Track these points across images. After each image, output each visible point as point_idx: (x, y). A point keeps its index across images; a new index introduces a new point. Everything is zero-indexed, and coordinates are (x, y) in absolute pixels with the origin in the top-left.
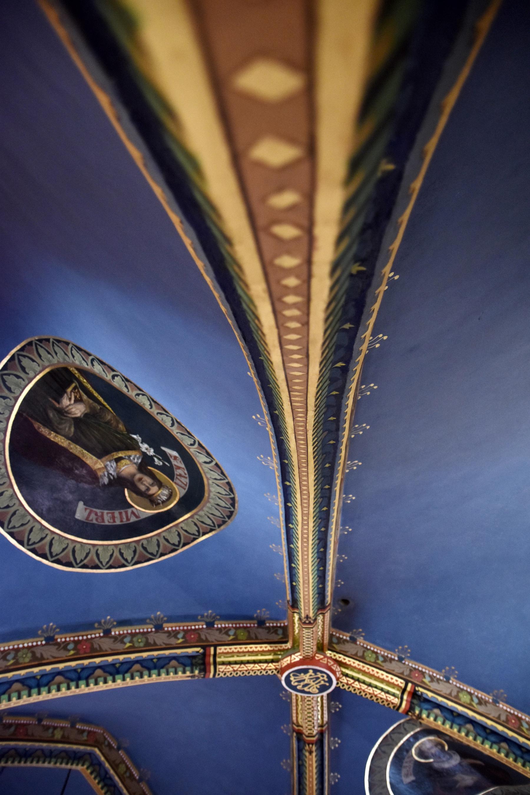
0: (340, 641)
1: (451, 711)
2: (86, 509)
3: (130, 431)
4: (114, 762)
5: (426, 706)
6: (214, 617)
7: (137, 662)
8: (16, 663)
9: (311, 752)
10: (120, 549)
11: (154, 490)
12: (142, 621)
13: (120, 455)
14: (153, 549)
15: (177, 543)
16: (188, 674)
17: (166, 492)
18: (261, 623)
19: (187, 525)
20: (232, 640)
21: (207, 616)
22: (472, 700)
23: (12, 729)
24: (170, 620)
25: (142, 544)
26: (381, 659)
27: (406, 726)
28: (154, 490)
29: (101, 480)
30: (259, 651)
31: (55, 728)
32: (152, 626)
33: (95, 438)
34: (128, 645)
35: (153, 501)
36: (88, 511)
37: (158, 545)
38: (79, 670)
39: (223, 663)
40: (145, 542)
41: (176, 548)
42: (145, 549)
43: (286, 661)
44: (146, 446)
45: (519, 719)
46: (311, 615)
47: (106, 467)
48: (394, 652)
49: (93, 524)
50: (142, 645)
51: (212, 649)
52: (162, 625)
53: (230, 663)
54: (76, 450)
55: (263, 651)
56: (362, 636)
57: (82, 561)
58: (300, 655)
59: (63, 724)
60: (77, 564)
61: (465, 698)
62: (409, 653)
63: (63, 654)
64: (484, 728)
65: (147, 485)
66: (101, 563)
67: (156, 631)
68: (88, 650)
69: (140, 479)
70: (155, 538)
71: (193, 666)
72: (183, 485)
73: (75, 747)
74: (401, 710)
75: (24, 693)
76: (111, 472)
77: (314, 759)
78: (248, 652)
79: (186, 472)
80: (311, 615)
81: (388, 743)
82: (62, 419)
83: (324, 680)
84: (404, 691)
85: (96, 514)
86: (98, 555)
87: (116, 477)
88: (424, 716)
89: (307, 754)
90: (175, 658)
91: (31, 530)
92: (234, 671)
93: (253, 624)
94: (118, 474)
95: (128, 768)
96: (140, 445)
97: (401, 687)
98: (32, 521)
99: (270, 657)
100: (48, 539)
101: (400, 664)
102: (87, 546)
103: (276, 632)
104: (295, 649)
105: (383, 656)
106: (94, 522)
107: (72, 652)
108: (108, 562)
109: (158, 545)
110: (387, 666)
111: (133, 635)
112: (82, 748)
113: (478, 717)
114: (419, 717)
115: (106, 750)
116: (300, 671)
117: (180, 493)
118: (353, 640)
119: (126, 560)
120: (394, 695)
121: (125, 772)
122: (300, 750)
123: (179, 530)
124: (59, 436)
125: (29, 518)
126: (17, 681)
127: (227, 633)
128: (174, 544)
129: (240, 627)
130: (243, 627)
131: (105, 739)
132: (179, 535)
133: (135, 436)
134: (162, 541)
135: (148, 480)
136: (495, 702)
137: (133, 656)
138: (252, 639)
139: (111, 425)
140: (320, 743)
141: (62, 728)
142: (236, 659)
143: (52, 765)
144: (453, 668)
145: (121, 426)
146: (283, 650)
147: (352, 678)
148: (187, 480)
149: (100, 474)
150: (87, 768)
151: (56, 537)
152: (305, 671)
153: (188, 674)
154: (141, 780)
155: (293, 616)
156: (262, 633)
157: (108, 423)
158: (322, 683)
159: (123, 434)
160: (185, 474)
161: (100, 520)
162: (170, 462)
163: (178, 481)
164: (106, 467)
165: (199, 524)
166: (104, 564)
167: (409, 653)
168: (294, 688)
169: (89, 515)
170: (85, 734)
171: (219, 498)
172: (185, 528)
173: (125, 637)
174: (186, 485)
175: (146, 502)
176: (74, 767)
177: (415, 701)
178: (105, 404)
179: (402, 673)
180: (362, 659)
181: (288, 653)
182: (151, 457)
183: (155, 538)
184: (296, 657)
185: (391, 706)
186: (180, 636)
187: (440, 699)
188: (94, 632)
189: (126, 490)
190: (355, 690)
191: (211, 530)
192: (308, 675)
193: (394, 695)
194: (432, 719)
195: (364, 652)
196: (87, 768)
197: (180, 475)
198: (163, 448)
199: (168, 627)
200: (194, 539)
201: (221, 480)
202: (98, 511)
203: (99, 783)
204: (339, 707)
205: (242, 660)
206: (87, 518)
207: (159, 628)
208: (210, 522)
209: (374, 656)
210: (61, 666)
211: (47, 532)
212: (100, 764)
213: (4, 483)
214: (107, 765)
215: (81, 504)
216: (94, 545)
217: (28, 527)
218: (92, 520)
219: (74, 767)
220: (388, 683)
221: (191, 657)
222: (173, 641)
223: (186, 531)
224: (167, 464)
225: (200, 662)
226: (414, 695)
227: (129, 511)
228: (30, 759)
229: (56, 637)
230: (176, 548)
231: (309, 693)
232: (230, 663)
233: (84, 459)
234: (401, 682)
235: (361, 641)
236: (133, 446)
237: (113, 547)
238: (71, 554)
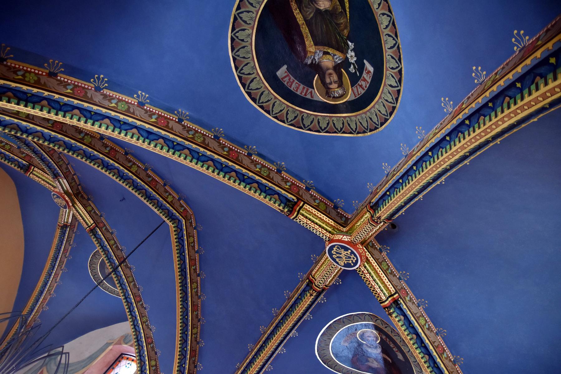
0: (373, 246)
1: (410, 322)
2: (286, 72)
3: (349, 38)
4: (189, 233)
5: (398, 311)
6: (312, 186)
7: (257, 182)
8: (193, 138)
9: (311, 295)
11: (334, 86)
12: (272, 162)
13: (329, 51)
14: (307, 122)
15: (323, 128)
16: (281, 208)
17: (340, 92)
18: (336, 207)
19: (337, 120)
20: (315, 205)
21: (308, 183)
22: (425, 324)
23: (150, 179)
24: (287, 171)
26: (389, 271)
27: (367, 317)
28: (334, 86)
29: (306, 59)
30: (326, 221)
31: (170, 194)
32: (276, 168)
33: (322, 30)
34: (258, 169)
35: (328, 93)
36: (286, 74)
38: (224, 166)
39: (303, 215)
40: (305, 115)
42: (302, 119)
43: (340, 237)
44: (353, 54)
45: (444, 351)
46: (383, 218)
47: (315, 53)
48: (399, 273)
49: (284, 85)
50: (265, 174)
51: (302, 203)
52: (281, 171)
53: (306, 217)
54: (305, 30)
55: (328, 223)
56: (387, 252)
57: (263, 103)
59: (175, 195)
61: (422, 322)
62: (407, 278)
63: (220, 151)
64: (422, 342)
66: (273, 111)
67: (276, 173)
68: (235, 158)
69: (330, 74)
70: (313, 117)
71: (286, 205)
72: (357, 94)
73: (174, 211)
74: (382, 305)
75: (189, 158)
76: (316, 58)
77: (310, 300)
78: (320, 218)
79: (368, 86)
80: (383, 218)
81: (350, 319)
82: (310, 5)
83: (352, 261)
84: (392, 295)
86: (274, 105)
88: (394, 315)
89: (309, 295)
90: (279, 194)
91: (247, 64)
92: (306, 223)
93: (332, 205)
94: (320, 62)
95: (194, 241)
96: (349, 51)
97: (391, 293)
98: (251, 58)
99: (330, 229)
100: (253, 76)
101: (398, 280)
103: (341, 218)
104: (347, 233)
105: (391, 270)
106: (285, 83)
107: (225, 153)
108: (276, 113)
110: (391, 277)
111: (263, 166)
112: (178, 214)
113: (423, 335)
114: (390, 314)
115: (188, 224)
116: (343, 247)
117: (349, 97)
118: (380, 251)
119: (287, 119)
120: (384, 294)
121: (192, 243)
122: (304, 291)
124: (300, 15)
125: (250, 55)
126: (188, 149)
127: (314, 200)
128: (321, 128)
129: (323, 202)
130: (325, 203)
131: (191, 219)
132: (328, 124)
133: (350, 43)
134: (316, 121)
135: (335, 77)
136: (437, 334)
137: (257, 178)
138: (326, 212)
139: (339, 27)
140: (319, 294)
141: (173, 197)
142: (311, 217)
143: (158, 213)
145: (346, 32)
146: (340, 230)
147: (368, 270)
148: (363, 92)
149: (309, 55)
150: (174, 227)
151: (258, 79)
152: (346, 249)
153: (281, 208)
154: (197, 252)
155: (365, 213)
156: (333, 213)
157: (338, 25)
158: (350, 262)
159: (342, 38)
160: (366, 87)
162: (361, 73)
163: (355, 89)
164: (315, 53)
165: (346, 124)
167: (407, 278)
168: (331, 255)
169: (285, 77)
170: (183, 209)
171: (376, 115)
172: (335, 122)
173: (258, 164)
174: (359, 94)
175: (324, 91)
176: (168, 222)
177: (394, 305)
178: (348, 10)
179: (397, 286)
180: (380, 264)
181: (341, 232)
182: (350, 64)
183: (313, 117)
184: (346, 238)
185: (379, 299)
186: (289, 184)
187: (409, 312)
188: (242, 150)
190: (364, 278)
191: (351, 133)
192: (346, 252)
193: (384, 294)
194: (397, 319)
195: (383, 261)
196: (174, 227)
197: (361, 86)
198: (365, 61)
199: (284, 174)
200: (335, 132)
201: (391, 103)
202: (292, 78)
203: (176, 238)
204: (339, 283)
205: (313, 220)
206: (282, 79)
207: (279, 172)
208: (354, 127)
209: (387, 267)
210: (216, 157)
211: (255, 71)
212: (181, 230)
213: (250, 24)
214: (185, 232)
215: (285, 67)
216: (276, 98)
217: (246, 61)
219: (168, 222)
220: (385, 286)
221: (288, 200)
222: (283, 184)
223: (334, 124)
224: (358, 73)
225: (291, 206)
226: (396, 302)
227: (310, 90)
228: (150, 201)
229: (221, 138)
231: (337, 263)
232: (306, 217)
233: (305, 40)
234: (393, 290)
235: (384, 254)
236: (343, 50)
238: (259, 94)
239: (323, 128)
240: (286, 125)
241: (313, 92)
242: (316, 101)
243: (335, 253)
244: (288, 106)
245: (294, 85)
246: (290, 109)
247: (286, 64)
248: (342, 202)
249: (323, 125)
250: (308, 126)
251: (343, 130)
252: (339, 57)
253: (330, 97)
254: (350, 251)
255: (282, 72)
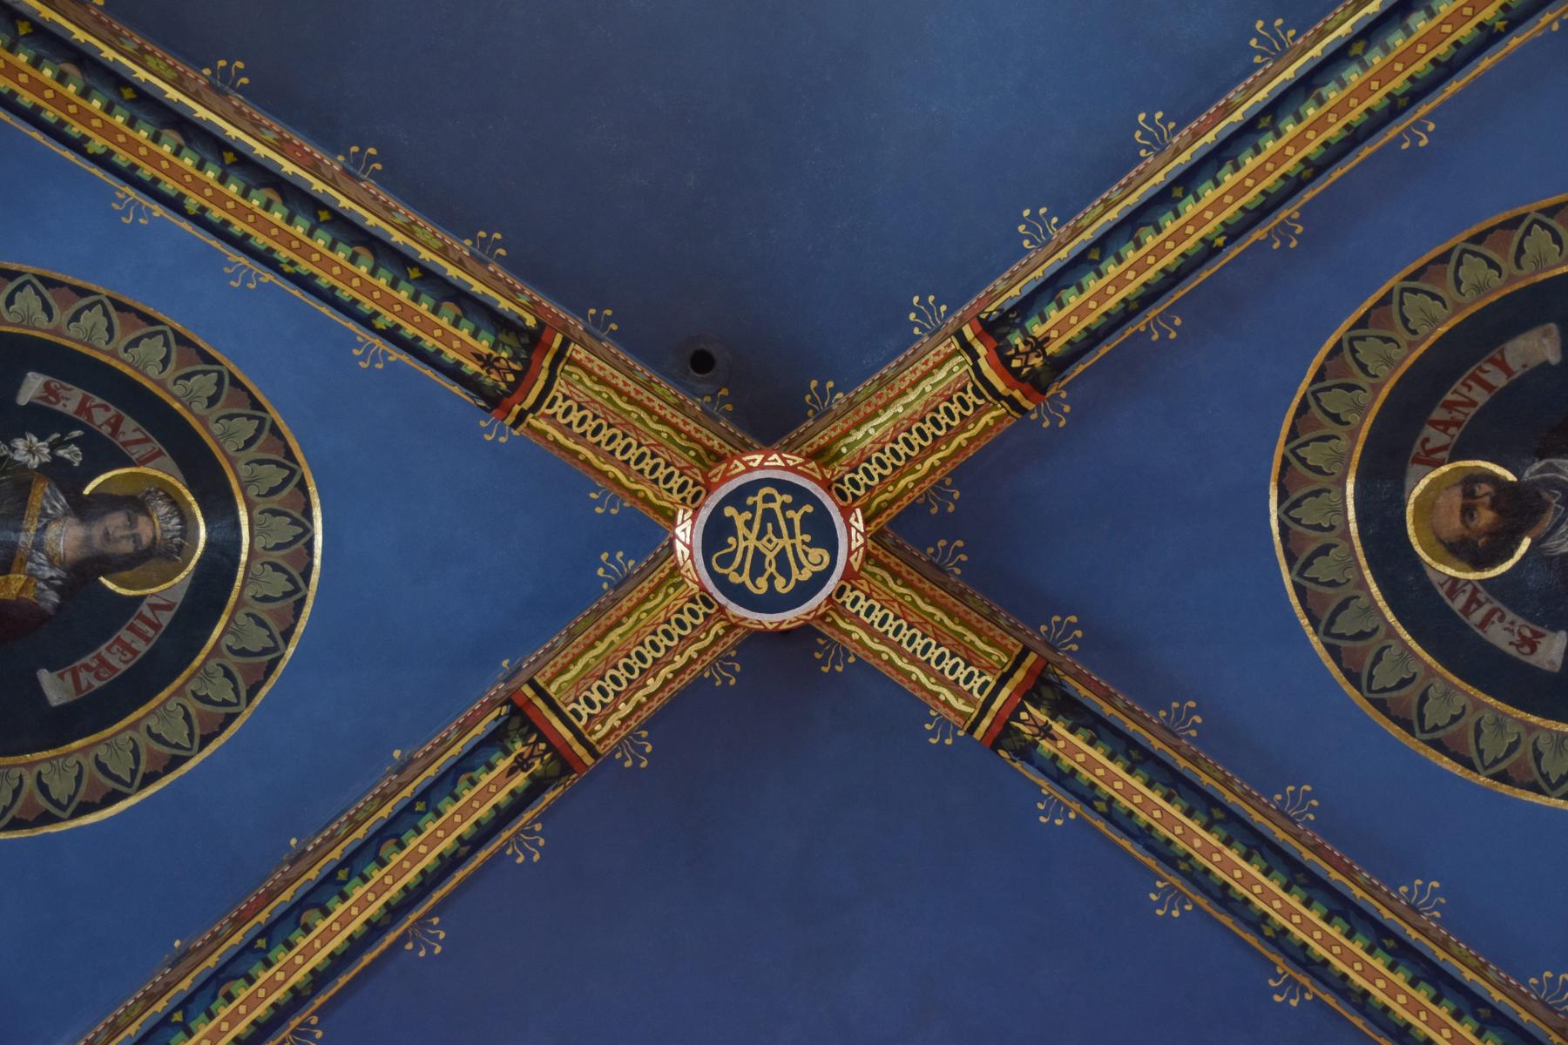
2: (61, 676)
10: (194, 693)
15: (290, 587)
17: (163, 509)
25: (229, 648)
29: (42, 604)
36: (68, 677)
37: (261, 623)
40: (230, 640)
41: (298, 596)
42: (243, 652)
56: (834, 391)
57: (134, 773)
58: (685, 511)
60: (129, 785)
65: (127, 533)
66: (178, 746)
83: (785, 507)
85: (87, 668)
86: (158, 738)
87: (64, 575)
102: (122, 736)
106: (97, 684)
108: (191, 735)
109: (261, 623)
119: (225, 703)
123: (266, 559)
128: (286, 595)
132: (276, 567)
134: (261, 609)
144: (1026, 213)
158: (796, 517)
161: (104, 673)
166: (187, 745)
167: (938, 303)
174: (147, 440)
189: (102, 579)
202: (87, 659)
215: (45, 676)
218: (90, 685)
223: (278, 547)
227: (144, 609)
230: (298, 596)
237: (175, 700)
239: (290, 587)
240: (247, 713)
241: (154, 600)
242: (187, 595)
243: (762, 583)
244: (179, 692)
245: (114, 661)
246: (191, 686)
247: (34, 670)
248: (611, 559)
249: (280, 584)
250: (271, 636)
251: (297, 515)
252: (44, 496)
253: (180, 546)
254: (729, 511)
255: (55, 689)
